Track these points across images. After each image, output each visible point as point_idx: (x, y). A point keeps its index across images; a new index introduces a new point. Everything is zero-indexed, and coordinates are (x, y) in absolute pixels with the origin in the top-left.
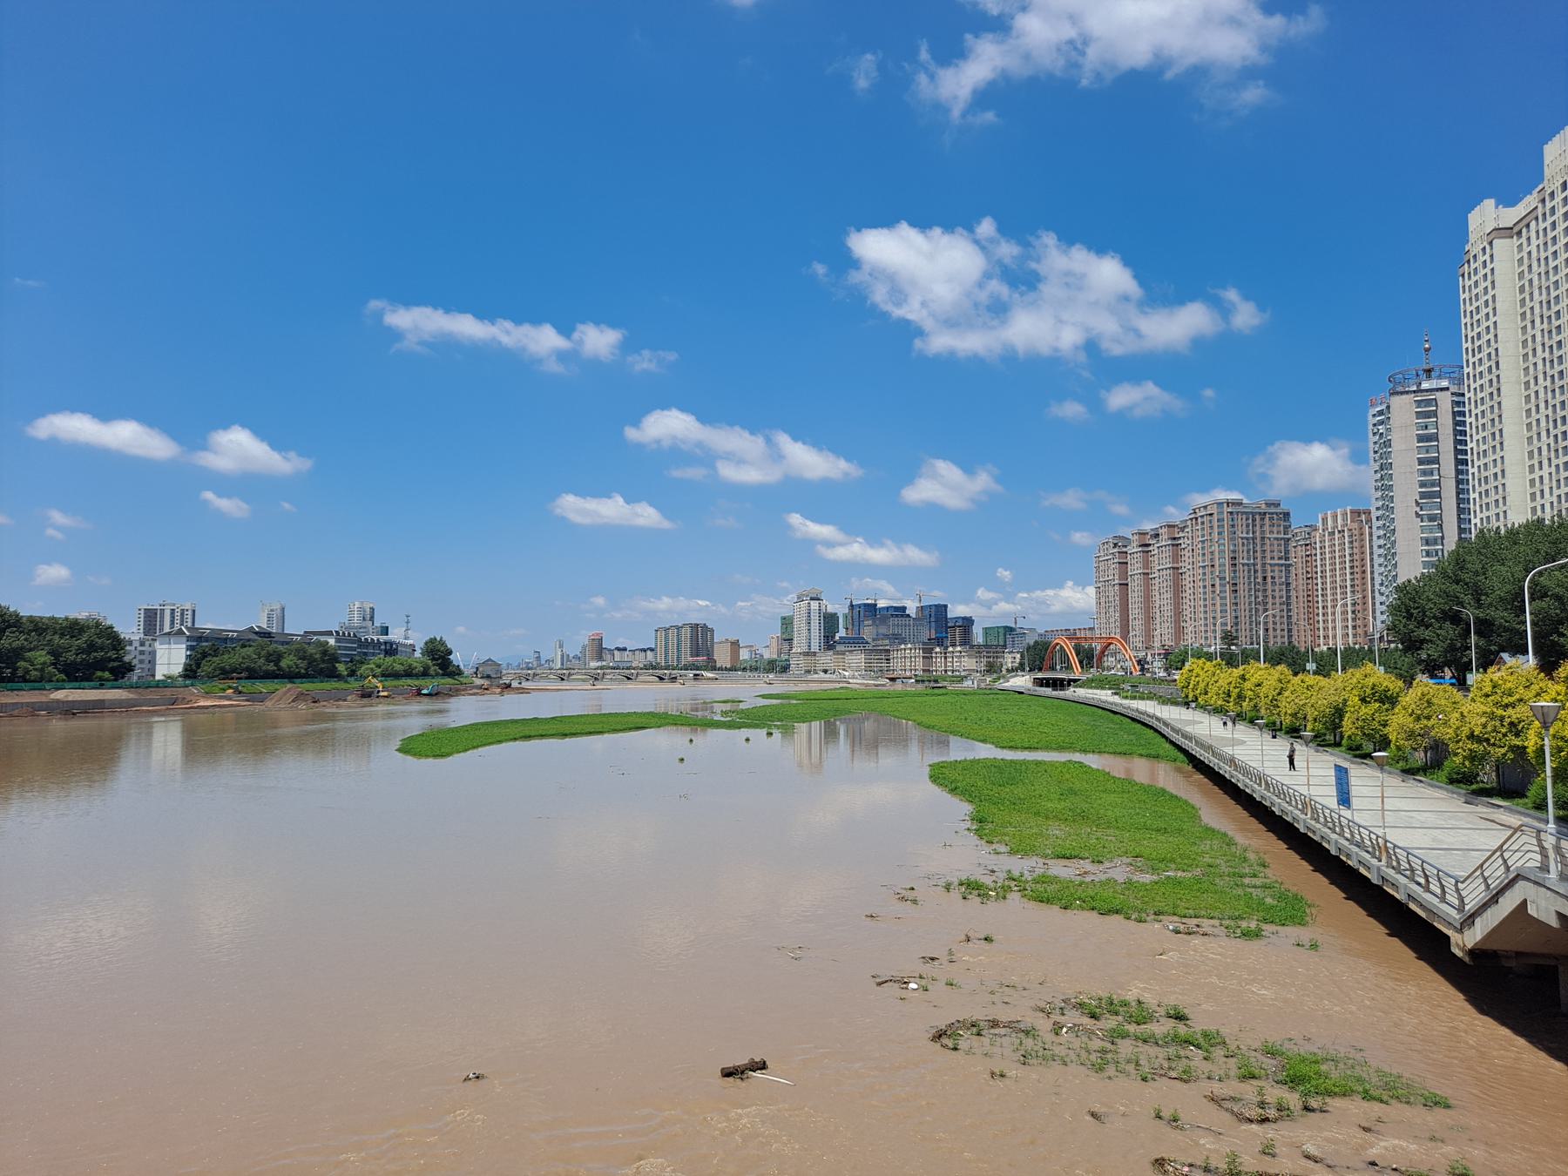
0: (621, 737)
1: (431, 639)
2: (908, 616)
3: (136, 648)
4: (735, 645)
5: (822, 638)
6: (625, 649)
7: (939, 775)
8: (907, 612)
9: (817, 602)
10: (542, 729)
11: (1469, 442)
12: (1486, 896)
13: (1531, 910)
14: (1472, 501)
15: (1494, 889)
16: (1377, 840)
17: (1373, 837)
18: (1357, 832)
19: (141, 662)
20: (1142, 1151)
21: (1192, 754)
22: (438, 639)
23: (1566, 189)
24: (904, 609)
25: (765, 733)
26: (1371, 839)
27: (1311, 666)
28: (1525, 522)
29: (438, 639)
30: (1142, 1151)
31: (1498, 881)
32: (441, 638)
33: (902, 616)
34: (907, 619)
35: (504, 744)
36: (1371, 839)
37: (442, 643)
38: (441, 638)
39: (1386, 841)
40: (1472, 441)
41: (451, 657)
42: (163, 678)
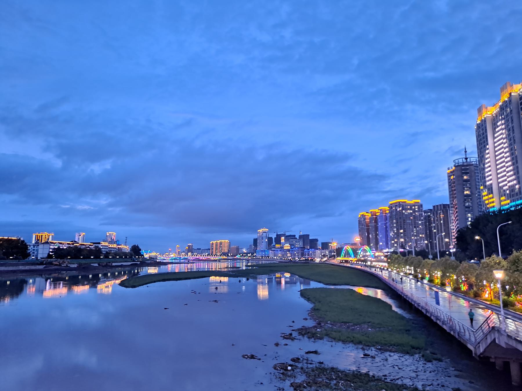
0: (197, 280)
1: (134, 245)
2: (296, 238)
3: (32, 248)
4: (315, 252)
5: (267, 245)
6: (200, 249)
7: (303, 294)
8: (296, 237)
9: (266, 233)
10: (170, 277)
11: (480, 182)
12: (483, 336)
13: (497, 341)
14: (482, 202)
15: (486, 333)
16: (448, 317)
17: (447, 316)
18: (442, 314)
19: (33, 253)
20: (352, 384)
21: (395, 290)
22: (136, 245)
23: (479, 126)
24: (295, 236)
25: (424, 206)
26: (446, 316)
27: (431, 256)
28: (498, 209)
29: (136, 245)
30: (352, 384)
31: (486, 331)
32: (137, 245)
33: (294, 238)
34: (296, 239)
35: (156, 283)
36: (446, 316)
37: (138, 247)
38: (137, 245)
39: (451, 317)
40: (481, 182)
41: (141, 252)
42: (40, 259)
